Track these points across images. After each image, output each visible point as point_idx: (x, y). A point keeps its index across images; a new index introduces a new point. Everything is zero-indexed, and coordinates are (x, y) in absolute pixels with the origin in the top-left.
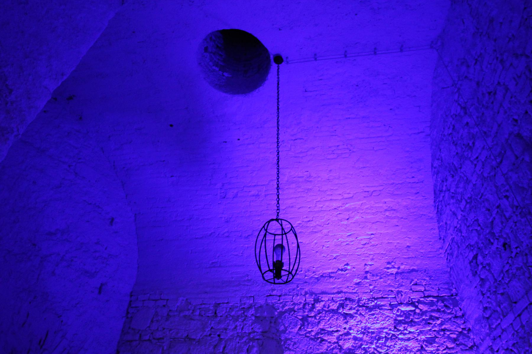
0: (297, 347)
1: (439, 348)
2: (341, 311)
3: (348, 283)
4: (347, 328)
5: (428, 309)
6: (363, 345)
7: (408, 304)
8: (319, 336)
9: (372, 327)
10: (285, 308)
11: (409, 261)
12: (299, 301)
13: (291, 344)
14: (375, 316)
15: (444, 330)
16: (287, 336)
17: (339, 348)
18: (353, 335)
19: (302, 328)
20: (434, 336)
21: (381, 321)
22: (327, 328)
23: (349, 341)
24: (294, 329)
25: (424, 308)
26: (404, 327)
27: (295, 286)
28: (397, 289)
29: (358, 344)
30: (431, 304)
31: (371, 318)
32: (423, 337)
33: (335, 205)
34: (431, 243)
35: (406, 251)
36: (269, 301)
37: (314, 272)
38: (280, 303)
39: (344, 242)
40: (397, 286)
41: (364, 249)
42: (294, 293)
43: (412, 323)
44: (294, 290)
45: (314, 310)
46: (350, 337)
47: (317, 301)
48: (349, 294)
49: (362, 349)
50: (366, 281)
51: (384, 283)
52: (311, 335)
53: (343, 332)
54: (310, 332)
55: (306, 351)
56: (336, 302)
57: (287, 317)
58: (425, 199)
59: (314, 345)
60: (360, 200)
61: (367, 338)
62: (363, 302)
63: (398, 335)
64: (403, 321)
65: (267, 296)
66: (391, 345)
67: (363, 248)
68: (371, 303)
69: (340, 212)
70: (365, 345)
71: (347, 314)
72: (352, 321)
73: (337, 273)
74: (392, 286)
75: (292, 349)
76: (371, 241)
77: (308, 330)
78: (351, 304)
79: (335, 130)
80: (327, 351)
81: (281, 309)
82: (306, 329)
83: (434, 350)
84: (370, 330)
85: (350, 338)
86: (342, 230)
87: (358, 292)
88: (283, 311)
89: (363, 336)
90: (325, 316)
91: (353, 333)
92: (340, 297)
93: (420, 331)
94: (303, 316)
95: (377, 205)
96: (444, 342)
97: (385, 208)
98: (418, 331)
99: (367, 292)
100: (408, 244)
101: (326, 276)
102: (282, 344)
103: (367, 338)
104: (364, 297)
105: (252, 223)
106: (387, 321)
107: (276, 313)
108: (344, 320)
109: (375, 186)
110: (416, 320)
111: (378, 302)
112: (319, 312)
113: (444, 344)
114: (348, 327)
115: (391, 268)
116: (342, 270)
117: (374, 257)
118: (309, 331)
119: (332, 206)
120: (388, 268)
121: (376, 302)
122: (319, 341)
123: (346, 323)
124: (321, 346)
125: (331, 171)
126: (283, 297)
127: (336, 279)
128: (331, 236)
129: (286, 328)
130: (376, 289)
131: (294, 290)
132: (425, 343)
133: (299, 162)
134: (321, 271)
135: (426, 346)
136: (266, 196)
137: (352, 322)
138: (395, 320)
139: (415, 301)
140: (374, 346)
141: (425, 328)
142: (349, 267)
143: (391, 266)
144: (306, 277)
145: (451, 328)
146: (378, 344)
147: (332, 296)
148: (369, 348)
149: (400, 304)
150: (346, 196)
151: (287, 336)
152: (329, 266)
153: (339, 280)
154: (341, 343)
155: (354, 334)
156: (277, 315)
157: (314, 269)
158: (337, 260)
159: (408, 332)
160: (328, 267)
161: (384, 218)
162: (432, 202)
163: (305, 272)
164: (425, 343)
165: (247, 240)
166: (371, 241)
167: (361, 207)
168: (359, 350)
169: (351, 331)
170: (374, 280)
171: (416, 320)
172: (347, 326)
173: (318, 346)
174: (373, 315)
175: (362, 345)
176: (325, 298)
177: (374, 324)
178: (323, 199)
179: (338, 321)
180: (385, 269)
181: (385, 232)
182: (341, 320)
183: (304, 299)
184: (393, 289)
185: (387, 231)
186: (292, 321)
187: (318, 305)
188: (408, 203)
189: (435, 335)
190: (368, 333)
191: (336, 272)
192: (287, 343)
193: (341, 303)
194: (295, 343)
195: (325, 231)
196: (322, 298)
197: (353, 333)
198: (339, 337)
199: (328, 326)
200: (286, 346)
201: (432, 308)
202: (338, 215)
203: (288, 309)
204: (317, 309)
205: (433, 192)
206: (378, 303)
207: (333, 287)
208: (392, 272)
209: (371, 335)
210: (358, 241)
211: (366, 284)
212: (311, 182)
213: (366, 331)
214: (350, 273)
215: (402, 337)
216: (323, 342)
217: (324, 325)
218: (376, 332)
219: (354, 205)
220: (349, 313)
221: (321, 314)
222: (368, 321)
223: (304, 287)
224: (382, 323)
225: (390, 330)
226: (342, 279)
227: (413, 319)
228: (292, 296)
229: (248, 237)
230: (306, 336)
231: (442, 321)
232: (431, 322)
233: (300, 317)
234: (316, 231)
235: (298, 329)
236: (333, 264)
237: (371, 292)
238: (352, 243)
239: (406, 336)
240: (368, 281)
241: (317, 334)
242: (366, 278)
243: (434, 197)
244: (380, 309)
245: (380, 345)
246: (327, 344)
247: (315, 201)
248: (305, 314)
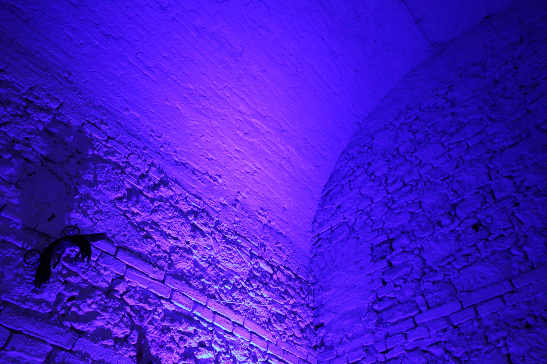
0: (101, 220)
1: (286, 331)
2: (191, 219)
3: (212, 195)
4: (191, 245)
5: (286, 281)
6: (204, 278)
7: (268, 263)
8: (146, 229)
9: (223, 262)
10: (110, 158)
11: (281, 223)
12: (138, 166)
13: (93, 209)
14: (231, 252)
15: (295, 313)
16: (92, 192)
17: (170, 262)
18: (195, 257)
19: (125, 200)
20: (284, 314)
21: (235, 263)
22: (163, 225)
23: (188, 261)
24: (109, 192)
25: (283, 279)
26: (258, 286)
27: (141, 146)
28: (262, 241)
29: (198, 273)
30: (289, 278)
31: (225, 252)
32: (274, 309)
33: (242, 107)
34: (304, 221)
35: (282, 211)
36: (87, 130)
37: (175, 152)
38: (104, 145)
39: (228, 151)
40: (263, 237)
41: (243, 176)
42: (136, 151)
43: (266, 286)
44: (137, 147)
45: (156, 192)
46: (191, 257)
47: (164, 183)
48: (208, 207)
49: (200, 282)
50: (233, 208)
51: (251, 225)
52: (134, 219)
53: (182, 245)
54: (133, 213)
55: (115, 235)
56: (190, 205)
57: (106, 169)
58: (321, 177)
59: (133, 236)
60: (268, 126)
61: (212, 273)
62: (222, 228)
63: (249, 291)
64: (259, 279)
65: (88, 121)
66: (238, 299)
67: (244, 174)
68: (231, 235)
69: (242, 120)
70: (206, 280)
71: (197, 227)
72: (202, 239)
73: (204, 176)
74: (258, 234)
75: (91, 216)
76: (255, 174)
77: (133, 209)
78: (207, 220)
79: (302, 37)
80: (149, 256)
81: (101, 154)
82: (129, 205)
83: (280, 331)
84: (220, 266)
85: (191, 259)
86: (233, 138)
87: (220, 212)
88: (104, 158)
89: (208, 267)
90: (167, 210)
91: (196, 256)
92: (195, 203)
93: (272, 300)
94: (134, 188)
95: (280, 146)
96: (293, 327)
97: (285, 156)
98: (271, 299)
99: (230, 221)
100: (285, 206)
101: (188, 168)
102: (75, 198)
103: (212, 273)
104: (225, 223)
105: (129, 29)
106: (243, 267)
107: (91, 153)
108: (191, 231)
109: (290, 127)
110: (271, 286)
111: (240, 240)
112: (161, 199)
113: (292, 329)
114: (193, 243)
115: (263, 216)
116: (211, 177)
117: (251, 193)
118: (133, 212)
119: (239, 107)
120: (260, 214)
121: (236, 238)
122: (143, 234)
123: (194, 237)
124: (143, 242)
125: (264, 71)
126: (114, 142)
127: (200, 180)
128: (218, 134)
129: (96, 183)
130: (241, 224)
131: (137, 147)
132: (274, 317)
133: (243, 28)
134: (185, 159)
135: (275, 322)
136: (173, 19)
137: (201, 241)
138: (251, 272)
139: (275, 265)
140: (216, 287)
141: (279, 300)
142: (220, 181)
143: (263, 214)
144: (162, 149)
145: (302, 315)
146: (223, 288)
147: (187, 194)
148: (210, 286)
149: (260, 257)
150: (259, 110)
151: (92, 192)
152: (199, 162)
153: (203, 184)
154: (174, 257)
155: (197, 258)
156: (90, 156)
157: (178, 149)
158: (211, 163)
159: (260, 294)
160: (196, 161)
161: (279, 164)
162: (323, 185)
163: (163, 142)
164: (274, 317)
165: (104, 38)
166: (255, 174)
167: (265, 134)
168: (197, 282)
169: (195, 252)
170: (242, 215)
171: (271, 286)
172: (193, 242)
173: (138, 239)
174: (229, 249)
175: (201, 277)
176: (178, 190)
177: (227, 262)
178: (236, 90)
179: (183, 228)
180: (257, 213)
181: (273, 177)
182: (188, 229)
183: (147, 169)
184: (258, 238)
185: (274, 178)
186: (113, 180)
187: (164, 189)
188: (305, 169)
189: (286, 314)
190: (215, 267)
191: (204, 174)
192: (87, 202)
193: (194, 210)
194: (100, 212)
195: (215, 123)
196: (172, 186)
197: (196, 256)
198: (176, 249)
199: (165, 224)
200: (81, 205)
201: (290, 283)
202: (238, 120)
203: (115, 162)
204: (160, 194)
205: (329, 177)
206: (238, 241)
207: (193, 186)
208: (262, 221)
209: (218, 271)
210: (243, 164)
211: (232, 212)
212: (237, 60)
213: (213, 262)
214: (219, 188)
215: (253, 296)
216: (149, 240)
217: (161, 220)
218: (226, 272)
219: (260, 126)
220: (201, 228)
221: (162, 203)
222: (221, 253)
223: (154, 157)
224: (236, 265)
225: (242, 279)
226: (207, 186)
227: (269, 283)
228: (129, 152)
229: (108, 36)
230: (124, 215)
231: (295, 302)
232: (286, 297)
233: (128, 186)
234: (205, 113)
235: (116, 196)
236: (205, 163)
237: (234, 223)
238: (236, 160)
239: (257, 298)
240: (236, 210)
241: (145, 223)
242: (235, 205)
243: (328, 182)
244: (238, 248)
245: (225, 291)
246: (153, 246)
247: (225, 84)
248: (138, 187)
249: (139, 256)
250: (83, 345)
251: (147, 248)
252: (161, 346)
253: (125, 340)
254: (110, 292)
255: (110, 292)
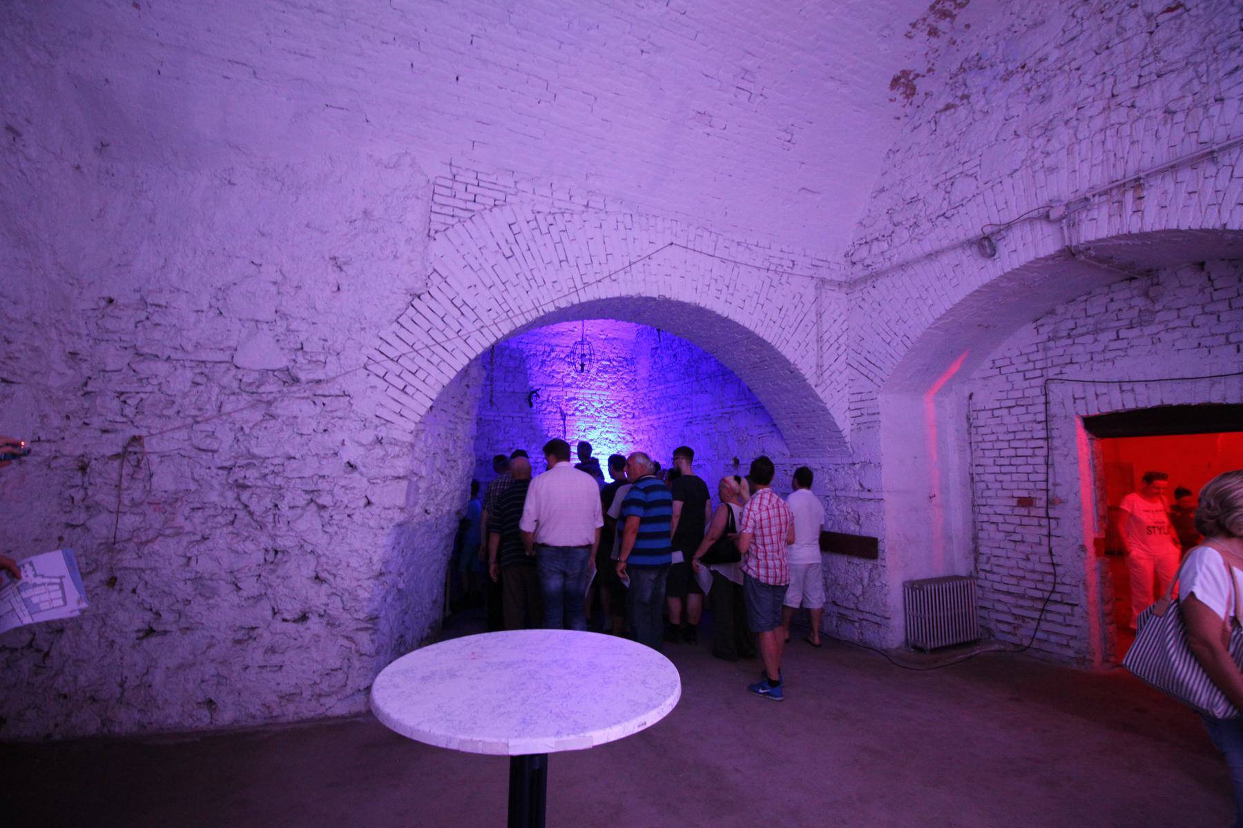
47: (552, 351)
112: (553, 359)
249: (553, 386)
250: (546, 416)
251: (554, 382)
252: (567, 410)
253: (556, 412)
254: (548, 400)
255: (548, 400)
